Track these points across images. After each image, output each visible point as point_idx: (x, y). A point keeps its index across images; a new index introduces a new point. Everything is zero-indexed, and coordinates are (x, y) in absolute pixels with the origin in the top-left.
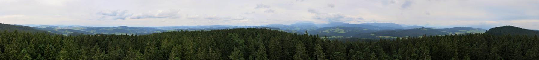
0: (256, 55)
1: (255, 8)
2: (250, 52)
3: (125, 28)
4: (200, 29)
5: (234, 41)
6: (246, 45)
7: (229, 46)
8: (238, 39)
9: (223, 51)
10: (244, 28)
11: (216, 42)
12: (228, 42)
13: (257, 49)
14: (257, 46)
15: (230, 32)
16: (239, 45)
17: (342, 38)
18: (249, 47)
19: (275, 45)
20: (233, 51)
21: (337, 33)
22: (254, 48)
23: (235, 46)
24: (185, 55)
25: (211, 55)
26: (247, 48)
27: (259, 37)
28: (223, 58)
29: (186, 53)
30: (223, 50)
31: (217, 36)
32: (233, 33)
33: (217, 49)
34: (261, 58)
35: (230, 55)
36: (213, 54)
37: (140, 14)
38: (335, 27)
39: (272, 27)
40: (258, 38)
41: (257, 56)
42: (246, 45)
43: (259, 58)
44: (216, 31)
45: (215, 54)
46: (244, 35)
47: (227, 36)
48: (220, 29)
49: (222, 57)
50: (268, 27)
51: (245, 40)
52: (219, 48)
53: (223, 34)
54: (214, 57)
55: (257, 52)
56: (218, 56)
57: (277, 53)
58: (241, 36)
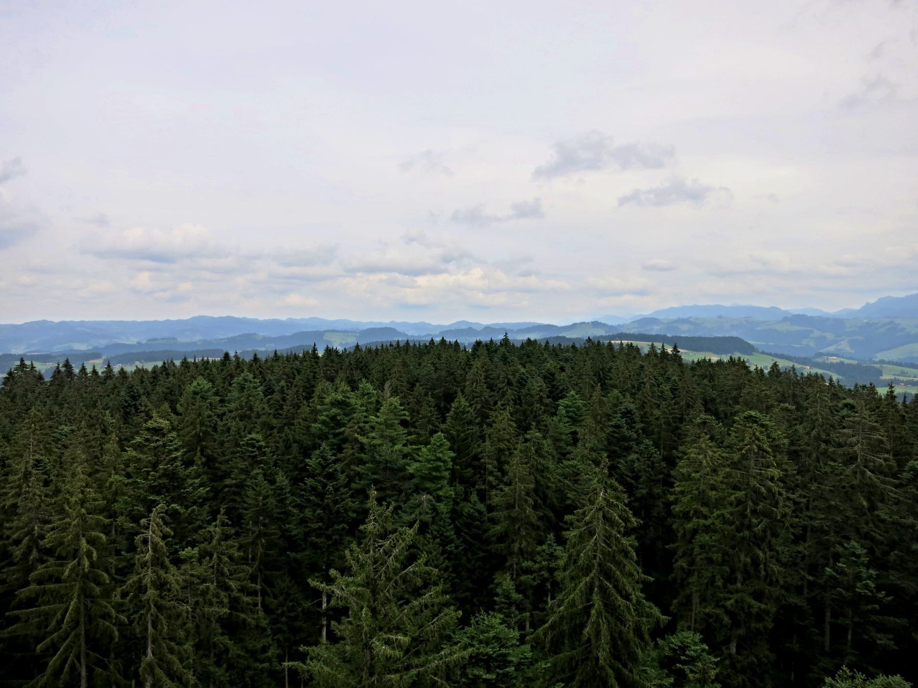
0: (551, 571)
1: (539, 173)
2: (502, 538)
3: (43, 326)
4: (44, 358)
5: (362, 448)
6: (462, 481)
7: (321, 496)
8: (401, 430)
9: (270, 545)
10: (450, 339)
11: (210, 461)
12: (312, 462)
13: (560, 517)
14: (564, 498)
15: (331, 379)
16: (407, 485)
18: (496, 499)
19: (740, 494)
20: (360, 537)
22: (535, 507)
23: (374, 493)
24: (31, 602)
25: (151, 592)
26: (473, 506)
27: (575, 420)
28: (273, 602)
29: (40, 582)
30: (273, 529)
31: (220, 410)
32: (353, 385)
33: (215, 529)
34: (596, 598)
35: (333, 572)
36: (174, 577)
37: (773, 352)
39: (685, 331)
40: (565, 428)
41: (559, 575)
42: (468, 483)
43: (575, 595)
44: (205, 368)
45: (199, 570)
46: (449, 397)
47: (305, 410)
48: (241, 350)
49: (264, 593)
50: (655, 330)
51: (459, 445)
52: (235, 518)
53: (269, 391)
54: (184, 601)
55: (561, 541)
56: (227, 588)
57: (756, 562)
58: (425, 410)
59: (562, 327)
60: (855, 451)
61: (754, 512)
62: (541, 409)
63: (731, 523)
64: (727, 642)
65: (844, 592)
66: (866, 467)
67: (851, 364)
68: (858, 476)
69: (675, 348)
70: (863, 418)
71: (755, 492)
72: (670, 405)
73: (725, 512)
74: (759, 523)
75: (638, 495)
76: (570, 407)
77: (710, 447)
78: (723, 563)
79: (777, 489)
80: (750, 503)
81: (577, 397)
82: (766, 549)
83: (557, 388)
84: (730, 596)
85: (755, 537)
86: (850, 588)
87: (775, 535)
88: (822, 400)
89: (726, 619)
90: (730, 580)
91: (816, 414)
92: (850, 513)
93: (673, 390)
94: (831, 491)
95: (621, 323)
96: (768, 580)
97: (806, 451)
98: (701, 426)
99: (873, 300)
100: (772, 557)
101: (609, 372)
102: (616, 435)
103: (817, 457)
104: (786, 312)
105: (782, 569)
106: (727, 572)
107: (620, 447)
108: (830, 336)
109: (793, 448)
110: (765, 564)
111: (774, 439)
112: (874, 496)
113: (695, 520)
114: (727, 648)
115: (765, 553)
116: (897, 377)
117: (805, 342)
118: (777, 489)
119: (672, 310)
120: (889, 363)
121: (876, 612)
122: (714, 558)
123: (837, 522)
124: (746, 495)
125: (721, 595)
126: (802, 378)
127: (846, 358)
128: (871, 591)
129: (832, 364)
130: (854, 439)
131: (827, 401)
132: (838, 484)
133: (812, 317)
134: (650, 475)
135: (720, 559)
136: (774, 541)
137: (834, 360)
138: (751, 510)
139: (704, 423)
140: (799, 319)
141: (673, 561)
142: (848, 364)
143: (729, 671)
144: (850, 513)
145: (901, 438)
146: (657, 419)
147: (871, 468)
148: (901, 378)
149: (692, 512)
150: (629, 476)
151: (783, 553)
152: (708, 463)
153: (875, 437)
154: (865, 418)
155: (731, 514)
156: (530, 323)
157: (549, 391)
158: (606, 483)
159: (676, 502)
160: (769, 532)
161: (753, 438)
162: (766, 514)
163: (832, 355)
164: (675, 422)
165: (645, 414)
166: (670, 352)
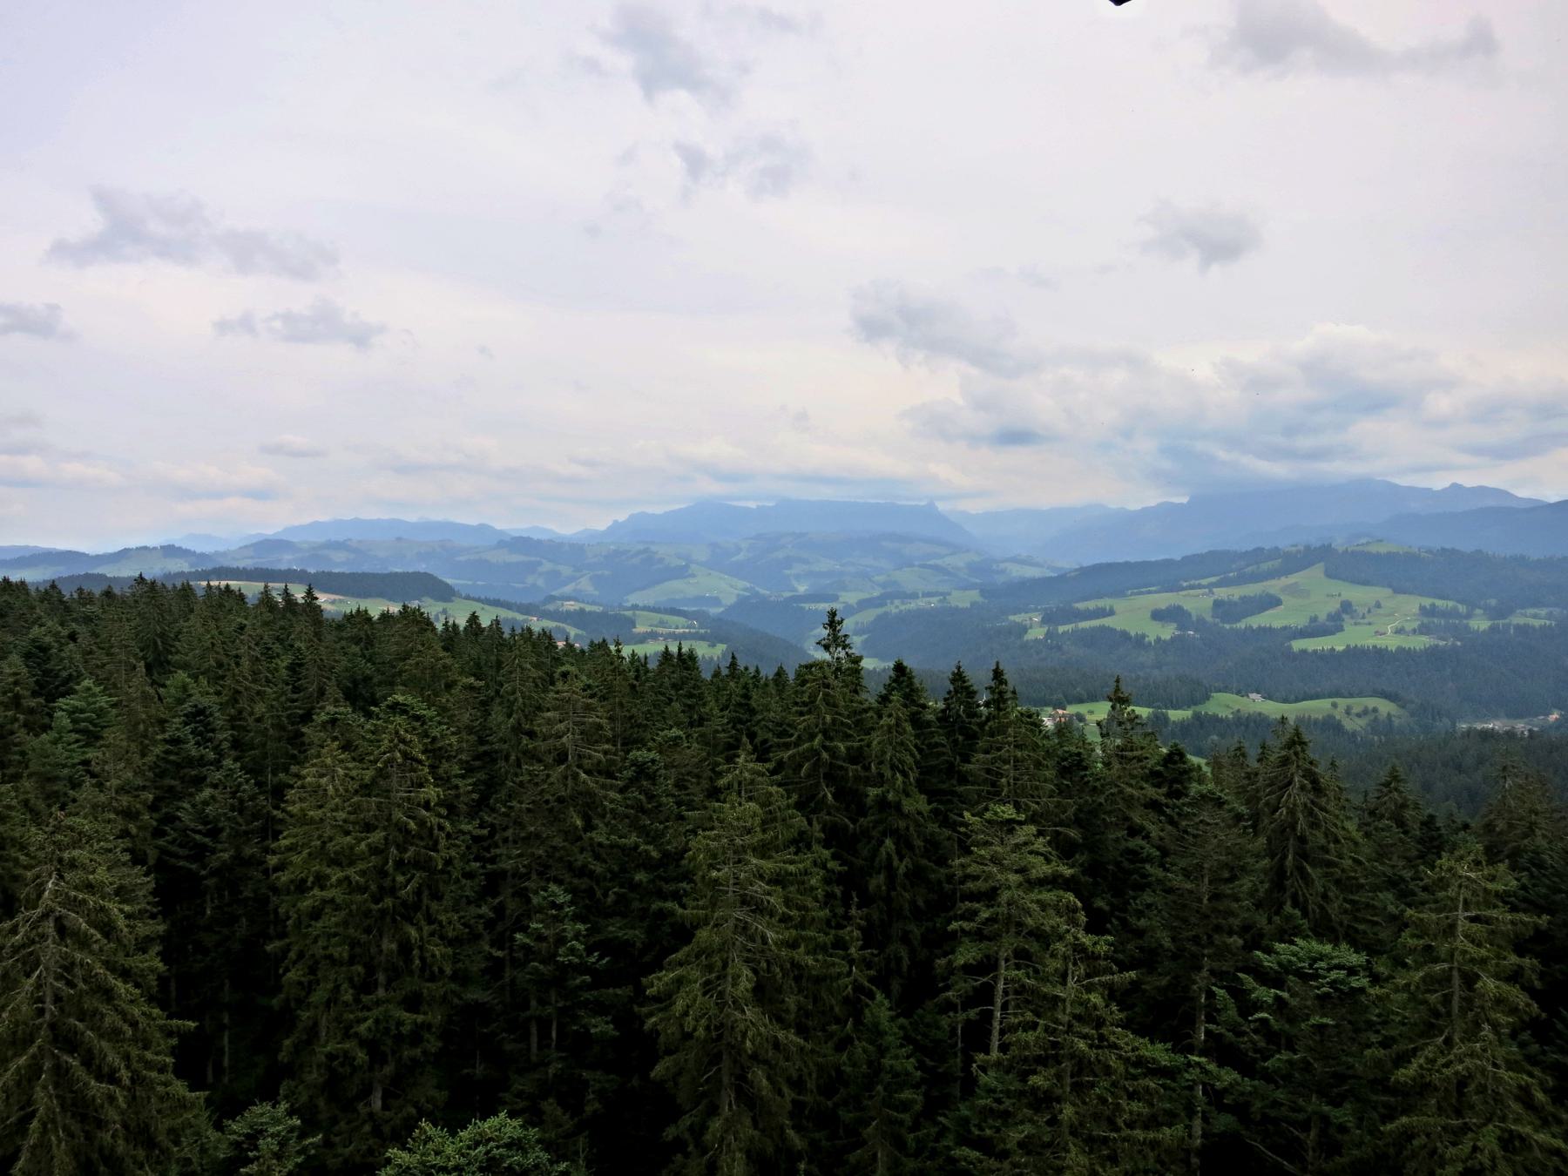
17: (1382, 727)
19: (377, 837)
21: (1297, 645)
34: (44, 1098)
38: (1258, 554)
39: (340, 564)
50: (286, 562)
57: (405, 948)
59: (98, 556)
60: (563, 744)
61: (400, 864)
62: (17, 720)
63: (362, 889)
64: (366, 1092)
65: (541, 967)
66: (579, 766)
67: (595, 612)
68: (570, 782)
69: (309, 593)
70: (574, 692)
71: (400, 830)
72: (284, 693)
73: (351, 872)
74: (409, 881)
75: (215, 864)
76: (82, 711)
77: (341, 761)
78: (352, 960)
79: (435, 820)
80: (393, 850)
81: (97, 690)
82: (423, 923)
83: (57, 676)
84: (366, 1014)
85: (404, 904)
86: (550, 958)
87: (438, 897)
88: (523, 669)
89: (361, 1056)
90: (366, 986)
91: (514, 693)
92: (558, 841)
93: (294, 668)
94: (529, 810)
95: (221, 549)
96: (427, 973)
97: (501, 751)
98: (329, 727)
99: (622, 517)
100: (432, 934)
101: (176, 638)
102: (172, 758)
103: (518, 760)
104: (501, 532)
105: (449, 950)
106: (359, 974)
107: (182, 780)
108: (566, 570)
109: (482, 749)
110: (421, 948)
111: (434, 739)
112: (590, 807)
113: (316, 892)
114: (366, 1105)
115: (420, 929)
116: (655, 629)
117: (530, 580)
118: (435, 820)
119: (315, 525)
120: (646, 608)
121: (585, 987)
122: (336, 955)
123: (540, 857)
124: (386, 839)
125: (352, 1016)
126: (513, 635)
127: (588, 603)
128: (580, 957)
129: (568, 612)
130: (561, 726)
131: (529, 670)
132: (539, 797)
133: (539, 542)
134: (237, 823)
135: (345, 955)
136: (434, 906)
137: (571, 606)
138: (394, 861)
139: (333, 721)
140: (521, 543)
141: (281, 971)
142: (590, 613)
143: (371, 1142)
144: (558, 841)
145: (631, 717)
146: (259, 720)
147: (586, 767)
148: (660, 630)
149: (311, 879)
150: (199, 832)
151: (450, 923)
152: (337, 790)
153: (591, 720)
154: (577, 694)
155: (363, 873)
156: (27, 548)
157: (37, 682)
158: (60, 860)
159: (280, 867)
160: (426, 894)
161: (396, 741)
162: (417, 864)
163: (569, 599)
164: (293, 724)
165: (240, 712)
166: (301, 601)
